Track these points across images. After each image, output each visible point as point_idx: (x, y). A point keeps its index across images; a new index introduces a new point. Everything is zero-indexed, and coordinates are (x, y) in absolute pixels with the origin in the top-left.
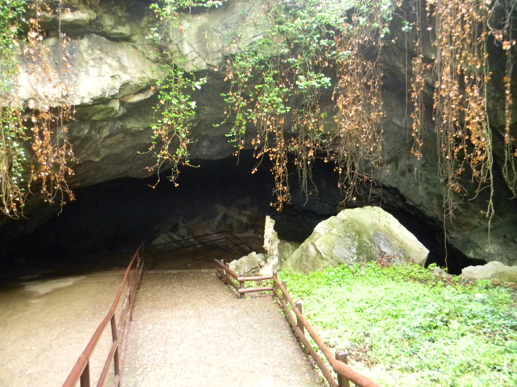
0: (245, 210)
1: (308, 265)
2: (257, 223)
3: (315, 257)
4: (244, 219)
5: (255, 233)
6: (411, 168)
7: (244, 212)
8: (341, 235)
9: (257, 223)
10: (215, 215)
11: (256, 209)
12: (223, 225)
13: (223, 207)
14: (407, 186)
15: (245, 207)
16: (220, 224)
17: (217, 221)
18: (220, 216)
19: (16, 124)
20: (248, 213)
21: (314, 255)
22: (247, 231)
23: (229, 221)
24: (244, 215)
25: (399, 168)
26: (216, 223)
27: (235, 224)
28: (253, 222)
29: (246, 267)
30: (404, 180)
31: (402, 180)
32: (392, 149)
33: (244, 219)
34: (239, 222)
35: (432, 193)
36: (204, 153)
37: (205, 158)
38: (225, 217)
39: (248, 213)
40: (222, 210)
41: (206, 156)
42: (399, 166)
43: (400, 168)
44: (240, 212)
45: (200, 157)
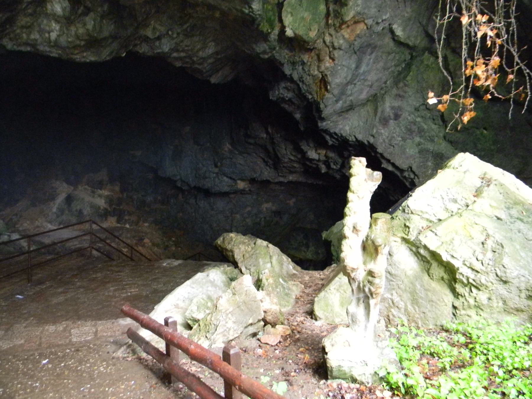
0: (101, 189)
1: (396, 299)
2: (121, 207)
3: (416, 278)
4: (101, 203)
5: (118, 222)
6: (400, 113)
7: (100, 192)
8: (503, 216)
9: (121, 207)
10: (53, 198)
11: (117, 188)
12: (67, 212)
13: (65, 185)
14: (390, 140)
15: (100, 185)
16: (61, 211)
17: (56, 206)
18: (60, 199)
19: (296, 394)
20: (106, 193)
21: (410, 273)
22: (106, 220)
23: (76, 206)
24: (100, 196)
25: (379, 114)
26: (54, 210)
27: (87, 211)
28: (114, 206)
29: (230, 324)
30: (384, 132)
31: (383, 131)
32: (377, 81)
33: (101, 203)
34: (93, 206)
35: (428, 151)
36: (53, 36)
37: (55, 53)
38: (69, 199)
39: (106, 193)
40: (63, 190)
41: (56, 45)
42: (380, 110)
43: (383, 112)
44: (93, 192)
45: (41, 48)
